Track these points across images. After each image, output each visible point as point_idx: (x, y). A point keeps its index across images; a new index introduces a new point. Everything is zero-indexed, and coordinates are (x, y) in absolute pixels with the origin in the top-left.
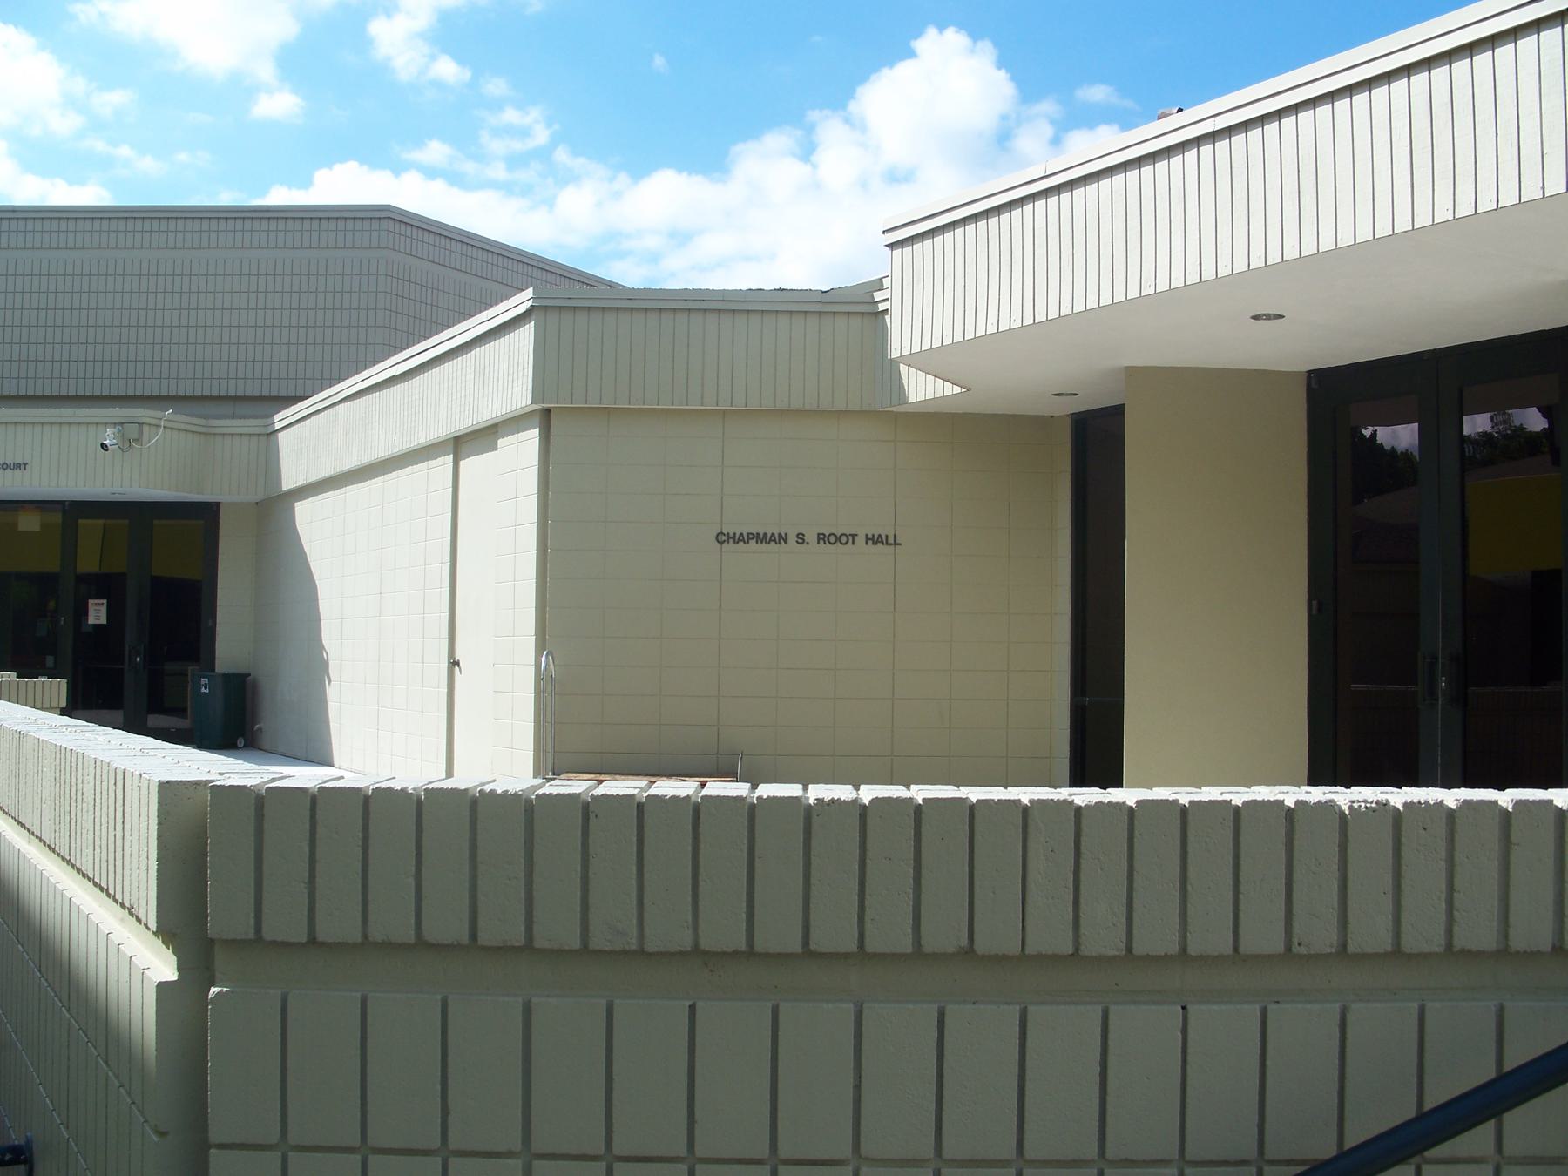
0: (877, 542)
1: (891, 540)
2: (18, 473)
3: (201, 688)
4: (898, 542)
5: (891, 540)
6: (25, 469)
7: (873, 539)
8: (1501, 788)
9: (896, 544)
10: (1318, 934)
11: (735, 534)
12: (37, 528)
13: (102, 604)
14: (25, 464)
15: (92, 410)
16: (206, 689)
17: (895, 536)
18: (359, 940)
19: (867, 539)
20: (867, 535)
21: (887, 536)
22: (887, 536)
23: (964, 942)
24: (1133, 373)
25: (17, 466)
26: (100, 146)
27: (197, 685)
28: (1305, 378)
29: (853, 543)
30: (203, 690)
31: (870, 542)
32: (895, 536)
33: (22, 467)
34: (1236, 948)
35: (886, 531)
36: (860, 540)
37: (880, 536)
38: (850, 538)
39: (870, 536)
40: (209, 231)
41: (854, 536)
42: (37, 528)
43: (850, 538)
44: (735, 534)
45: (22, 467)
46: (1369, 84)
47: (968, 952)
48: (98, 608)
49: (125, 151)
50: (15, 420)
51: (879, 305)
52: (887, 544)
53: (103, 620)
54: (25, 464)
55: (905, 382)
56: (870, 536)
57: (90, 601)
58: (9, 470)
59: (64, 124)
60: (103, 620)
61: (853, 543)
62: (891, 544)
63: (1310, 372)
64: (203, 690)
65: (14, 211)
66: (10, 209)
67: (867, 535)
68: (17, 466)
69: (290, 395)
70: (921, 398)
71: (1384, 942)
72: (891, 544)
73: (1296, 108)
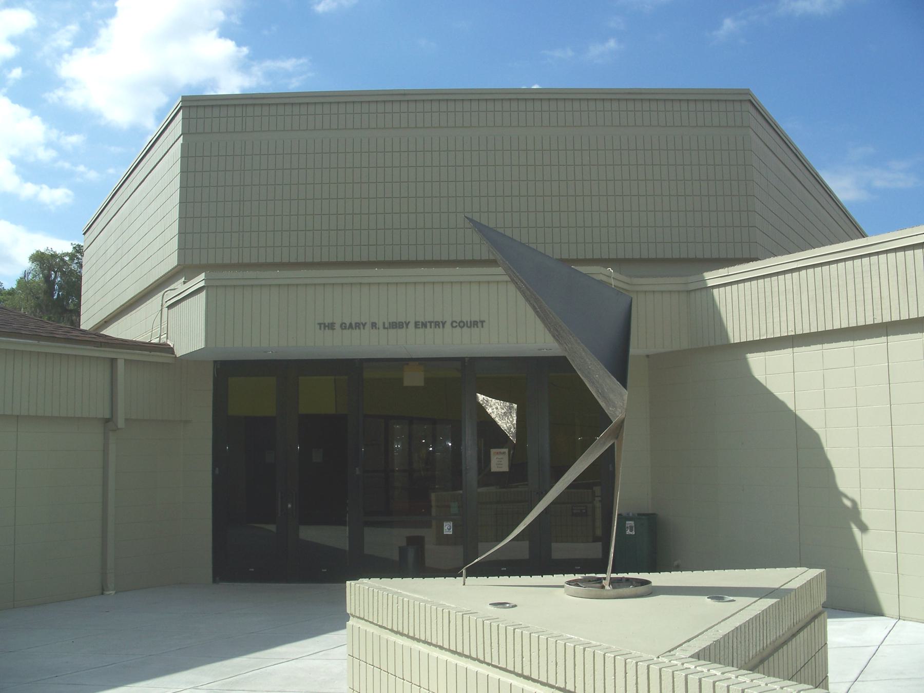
1: (322, 326)
2: (475, 330)
3: (625, 531)
6: (482, 327)
12: (421, 383)
13: (504, 453)
14: (482, 322)
15: (415, 270)
16: (631, 531)
22: (431, 327)
25: (474, 324)
26: (67, 165)
30: (628, 532)
33: (479, 325)
40: (408, 151)
42: (421, 383)
45: (479, 325)
48: (500, 456)
49: (81, 168)
50: (462, 279)
53: (505, 468)
54: (482, 322)
57: (491, 450)
58: (465, 327)
59: (45, 155)
60: (505, 468)
62: (386, 328)
64: (628, 532)
65: (405, 94)
66: (403, 92)
68: (474, 324)
69: (475, 258)
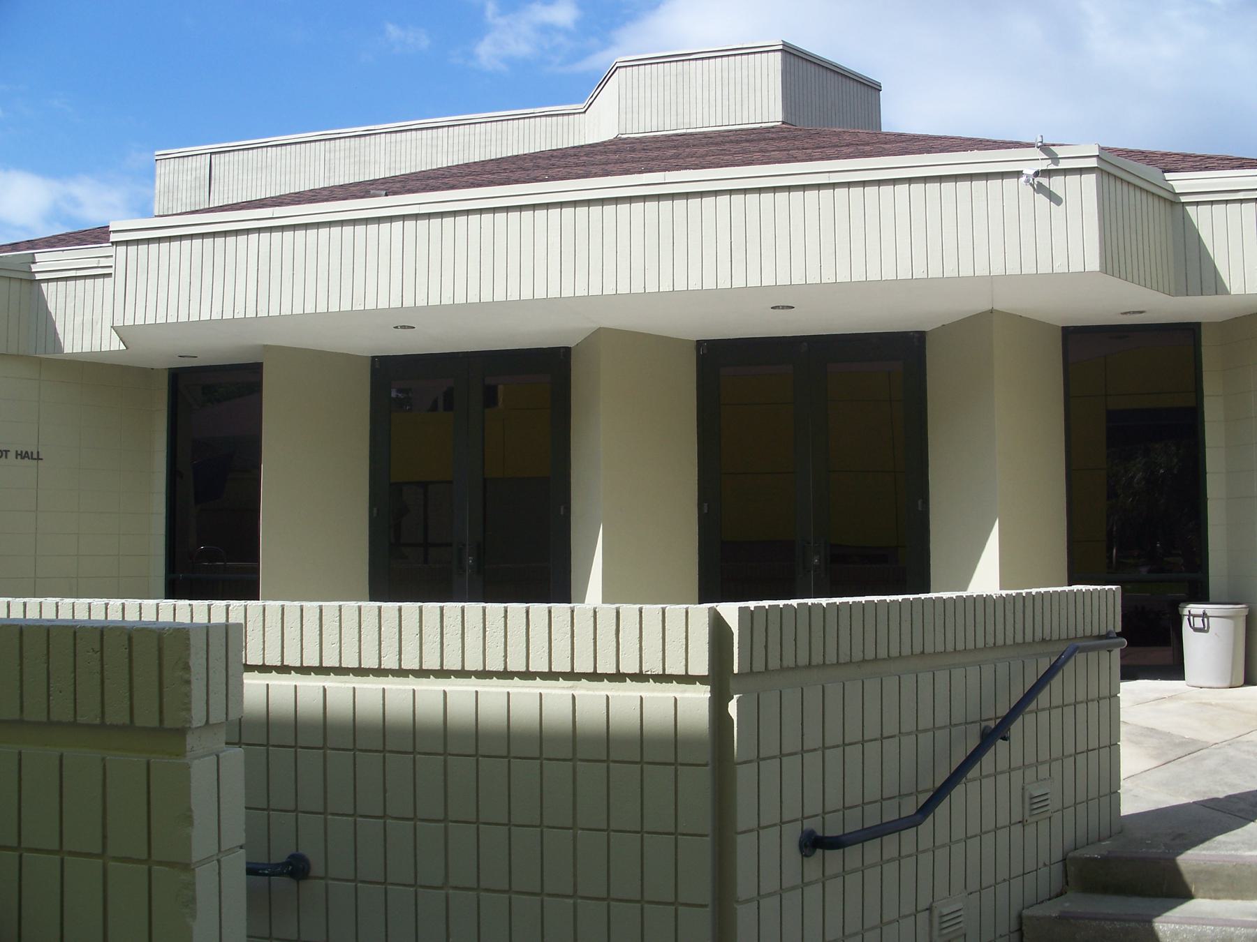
0: (25, 457)
1: (35, 456)
4: (40, 457)
5: (35, 456)
7: (21, 455)
8: (1023, 589)
9: (38, 459)
10: (970, 646)
11: (22, 452)
17: (38, 452)
18: (684, 674)
19: (17, 454)
20: (17, 451)
21: (32, 453)
23: (874, 656)
24: (266, 348)
27: (819, 560)
28: (369, 362)
29: (6, 457)
31: (19, 457)
32: (38, 452)
34: (975, 647)
35: (30, 448)
36: (12, 455)
37: (27, 452)
38: (4, 453)
39: (19, 452)
41: (7, 451)
43: (4, 453)
44: (22, 452)
46: (575, 204)
47: (1076, 637)
51: (36, 275)
52: (32, 459)
55: (61, 337)
56: (19, 452)
61: (6, 457)
62: (35, 459)
63: (373, 358)
67: (17, 451)
70: (77, 349)
71: (1066, 637)
72: (35, 459)
73: (521, 208)
